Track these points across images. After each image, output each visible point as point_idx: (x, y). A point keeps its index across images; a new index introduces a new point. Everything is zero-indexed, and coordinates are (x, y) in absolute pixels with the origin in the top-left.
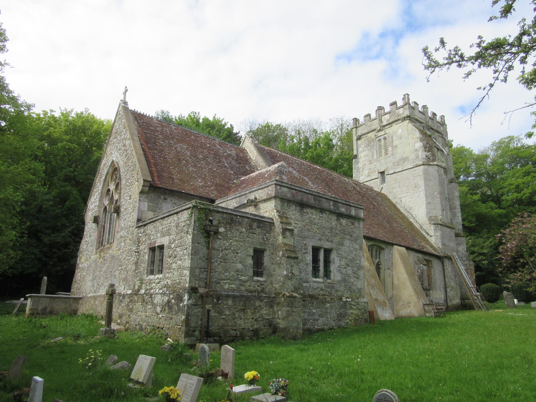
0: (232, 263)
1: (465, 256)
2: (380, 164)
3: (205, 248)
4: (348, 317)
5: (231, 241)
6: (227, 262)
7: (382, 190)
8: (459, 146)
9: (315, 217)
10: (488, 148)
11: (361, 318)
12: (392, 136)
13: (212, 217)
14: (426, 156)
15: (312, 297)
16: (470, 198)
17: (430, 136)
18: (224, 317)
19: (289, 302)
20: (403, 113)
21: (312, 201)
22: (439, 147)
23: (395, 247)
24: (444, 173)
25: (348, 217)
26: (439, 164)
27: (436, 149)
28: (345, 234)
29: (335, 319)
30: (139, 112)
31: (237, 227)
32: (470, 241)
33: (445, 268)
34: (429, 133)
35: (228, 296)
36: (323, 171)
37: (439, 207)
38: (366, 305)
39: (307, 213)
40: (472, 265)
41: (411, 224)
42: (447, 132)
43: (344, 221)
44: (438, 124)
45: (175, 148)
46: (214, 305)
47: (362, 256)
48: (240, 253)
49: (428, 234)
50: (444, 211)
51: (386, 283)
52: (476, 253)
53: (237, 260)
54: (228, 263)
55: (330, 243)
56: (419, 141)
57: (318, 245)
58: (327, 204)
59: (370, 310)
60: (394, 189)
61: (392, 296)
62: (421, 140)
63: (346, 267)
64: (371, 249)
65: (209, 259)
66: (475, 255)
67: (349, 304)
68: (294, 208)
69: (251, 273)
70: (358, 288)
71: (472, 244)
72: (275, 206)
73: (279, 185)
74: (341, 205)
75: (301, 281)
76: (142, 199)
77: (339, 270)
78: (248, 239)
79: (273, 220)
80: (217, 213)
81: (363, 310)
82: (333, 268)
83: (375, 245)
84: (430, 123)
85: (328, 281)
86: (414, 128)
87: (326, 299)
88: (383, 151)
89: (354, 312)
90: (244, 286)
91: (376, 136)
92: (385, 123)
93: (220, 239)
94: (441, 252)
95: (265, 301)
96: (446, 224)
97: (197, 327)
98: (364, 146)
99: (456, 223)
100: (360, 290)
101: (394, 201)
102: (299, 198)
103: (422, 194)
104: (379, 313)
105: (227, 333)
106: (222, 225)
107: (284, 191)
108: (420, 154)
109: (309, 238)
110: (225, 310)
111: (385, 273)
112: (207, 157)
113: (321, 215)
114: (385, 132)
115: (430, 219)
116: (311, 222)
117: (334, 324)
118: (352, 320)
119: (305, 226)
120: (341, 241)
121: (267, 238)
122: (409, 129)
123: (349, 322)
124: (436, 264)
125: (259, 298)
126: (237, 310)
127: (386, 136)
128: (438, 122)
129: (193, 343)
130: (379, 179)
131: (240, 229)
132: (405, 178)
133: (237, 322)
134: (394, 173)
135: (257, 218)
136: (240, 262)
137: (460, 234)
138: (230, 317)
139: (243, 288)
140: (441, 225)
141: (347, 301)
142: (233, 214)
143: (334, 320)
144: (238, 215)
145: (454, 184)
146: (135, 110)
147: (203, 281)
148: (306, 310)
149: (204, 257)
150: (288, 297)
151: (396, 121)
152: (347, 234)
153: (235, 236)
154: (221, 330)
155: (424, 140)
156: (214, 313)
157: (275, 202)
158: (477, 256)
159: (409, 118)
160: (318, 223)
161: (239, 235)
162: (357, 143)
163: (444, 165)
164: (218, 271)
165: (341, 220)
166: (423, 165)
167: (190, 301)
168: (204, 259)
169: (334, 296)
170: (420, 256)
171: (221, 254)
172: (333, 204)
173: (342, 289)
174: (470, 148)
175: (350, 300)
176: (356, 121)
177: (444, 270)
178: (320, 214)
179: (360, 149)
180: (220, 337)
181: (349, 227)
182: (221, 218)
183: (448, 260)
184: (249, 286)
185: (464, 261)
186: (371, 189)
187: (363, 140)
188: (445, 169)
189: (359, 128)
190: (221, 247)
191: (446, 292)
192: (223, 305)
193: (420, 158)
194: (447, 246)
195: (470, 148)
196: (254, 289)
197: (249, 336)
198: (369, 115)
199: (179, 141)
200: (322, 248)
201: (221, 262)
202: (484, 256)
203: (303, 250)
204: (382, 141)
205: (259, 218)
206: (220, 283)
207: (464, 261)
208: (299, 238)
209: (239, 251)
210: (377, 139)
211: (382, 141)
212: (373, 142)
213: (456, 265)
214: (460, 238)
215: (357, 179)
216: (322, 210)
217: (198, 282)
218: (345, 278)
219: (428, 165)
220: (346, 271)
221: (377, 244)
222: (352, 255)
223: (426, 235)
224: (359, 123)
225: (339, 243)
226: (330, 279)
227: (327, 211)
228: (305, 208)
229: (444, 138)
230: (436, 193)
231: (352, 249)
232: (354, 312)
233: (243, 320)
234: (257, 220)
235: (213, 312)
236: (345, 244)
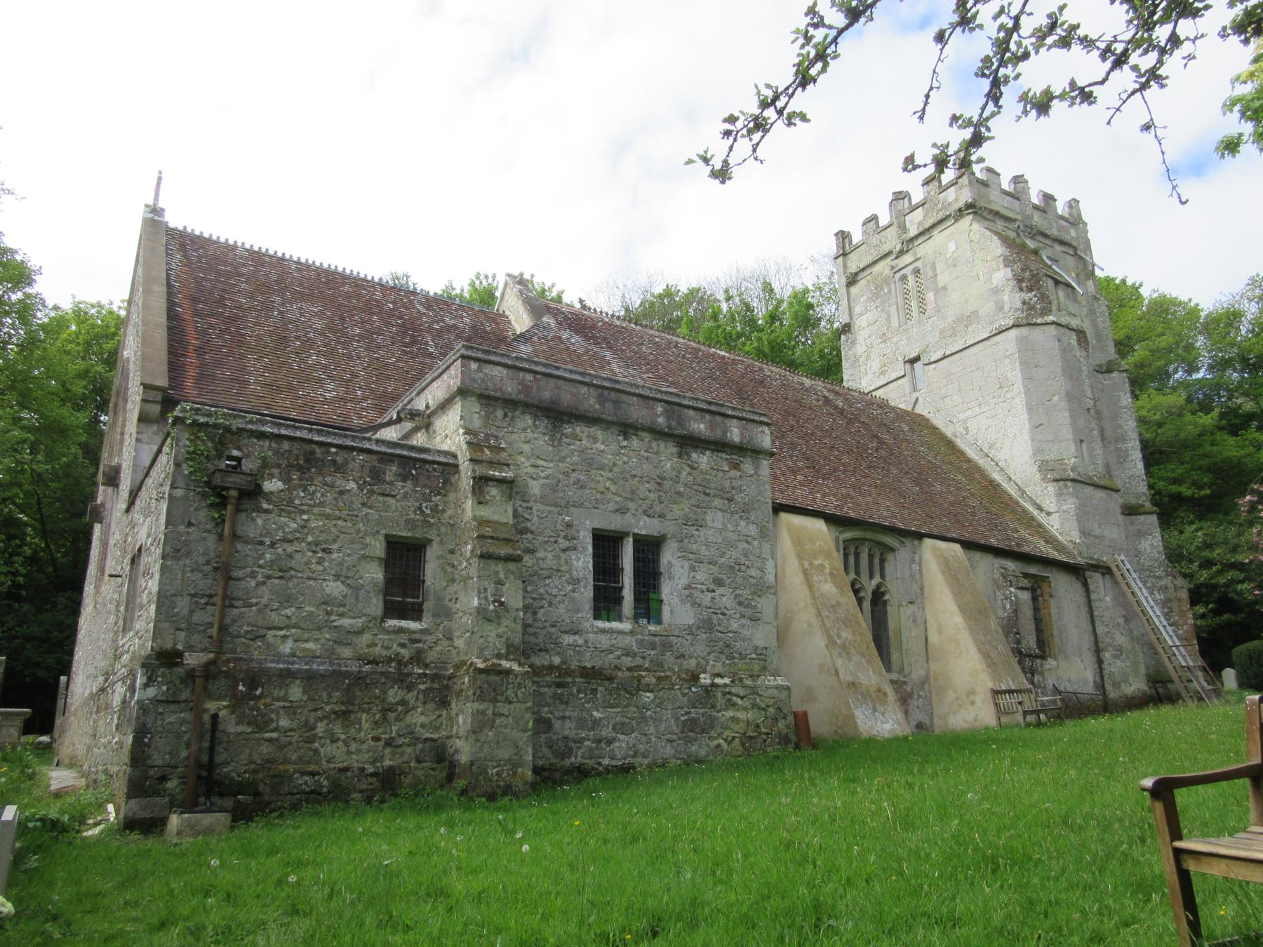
0: (309, 578)
1: (1159, 566)
2: (908, 339)
3: (212, 538)
4: (719, 730)
5: (305, 517)
6: (292, 577)
7: (917, 406)
8: (1156, 295)
9: (602, 447)
10: (1242, 297)
11: (766, 734)
12: (934, 263)
13: (239, 448)
14: (1024, 303)
15: (591, 674)
16: (1190, 423)
17: (1036, 252)
18: (274, 735)
19: (485, 686)
20: (956, 200)
21: (590, 401)
22: (1061, 276)
23: (928, 542)
24: (1079, 344)
25: (720, 446)
26: (1064, 320)
27: (1050, 283)
28: (708, 495)
29: (675, 737)
30: (197, 233)
31: (328, 479)
32: (1199, 534)
33: (1093, 597)
34: (1031, 244)
35: (287, 676)
36: (734, 362)
37: (1067, 433)
38: (783, 695)
39: (575, 437)
40: (1182, 588)
41: (993, 486)
42: (1088, 243)
43: (704, 460)
44: (1062, 222)
45: (281, 313)
46: (237, 703)
47: (769, 557)
48: (339, 550)
49: (1040, 509)
50: (1084, 446)
51: (904, 641)
52: (1216, 564)
53: (325, 569)
54: (295, 581)
55: (655, 521)
56: (1002, 265)
57: (613, 527)
58: (644, 412)
59: (794, 710)
60: (947, 401)
61: (927, 678)
62: (1007, 262)
63: (712, 587)
64: (852, 549)
65: (224, 571)
66: (1214, 569)
67: (724, 694)
68: (530, 422)
69: (376, 606)
70: (756, 648)
71: (1204, 543)
72: (462, 418)
73: (477, 360)
74: (691, 412)
75: (553, 630)
76: (144, 437)
77: (690, 596)
78: (365, 510)
79: (455, 456)
80: (257, 438)
81: (771, 710)
82: (669, 591)
83: (865, 539)
84: (1037, 219)
85: (652, 628)
86: (988, 233)
87: (639, 678)
88: (914, 304)
89: (741, 715)
90: (350, 644)
91: (892, 268)
92: (913, 232)
93: (267, 511)
94: (1080, 553)
95: (422, 687)
96: (1091, 478)
97: (176, 767)
98: (865, 297)
99: (1129, 478)
100: (762, 654)
101: (948, 431)
102: (546, 395)
103: (1019, 403)
104: (859, 722)
105: (282, 783)
106: (276, 471)
107: (492, 377)
108: (1006, 298)
109: (581, 506)
110: (278, 714)
111: (898, 615)
112: (376, 333)
113: (625, 443)
114: (915, 254)
115: (1044, 467)
116: (590, 463)
117: (669, 750)
118: (734, 738)
119: (566, 474)
120: (695, 513)
121: (435, 509)
122: (975, 237)
123: (724, 745)
124: (1064, 590)
125: (403, 680)
126: (319, 713)
127: (919, 264)
128: (1062, 218)
129: (157, 814)
130: (906, 378)
131: (338, 483)
132: (973, 368)
133: (322, 751)
134: (945, 357)
135: (398, 451)
136: (337, 577)
137: (1142, 506)
138: (296, 737)
139: (347, 652)
140: (1073, 480)
141: (713, 685)
142: (311, 442)
143: (671, 741)
144: (331, 445)
145: (1115, 374)
146: (185, 228)
147: (204, 631)
148: (567, 714)
149: (208, 563)
150: (485, 671)
151: (941, 221)
152: (715, 496)
153: (322, 504)
154: (261, 776)
155: (1014, 262)
156: (237, 724)
157: (463, 406)
158: (1220, 572)
159: (971, 208)
160: (615, 464)
161: (335, 499)
162: (848, 293)
163: (1075, 323)
164: (257, 604)
165: (694, 456)
167: (151, 692)
168: (208, 568)
169: (670, 669)
170: (1011, 565)
171: (268, 556)
172: (666, 411)
173: (700, 649)
174: (1190, 300)
175: (727, 680)
176: (843, 239)
177: (1089, 601)
178: (621, 438)
179: (858, 309)
180: (257, 794)
181: (721, 474)
182: (270, 453)
183: (1103, 574)
184: (368, 646)
185: (1160, 578)
186: (883, 405)
187: (862, 283)
188: (1080, 333)
189: (851, 255)
190: (268, 533)
191: (1100, 662)
192: (268, 700)
193: (1006, 308)
194: (1096, 537)
195: (1190, 300)
196: (385, 653)
197: (361, 791)
198: (874, 219)
199: (299, 297)
200: (627, 534)
201: (269, 577)
202: (1241, 570)
203: (561, 540)
204: (909, 278)
205: (405, 453)
206: (264, 636)
207: (1160, 578)
208: (549, 508)
209: (334, 547)
210: (898, 276)
211: (911, 278)
212: (888, 284)
213: (1125, 588)
214: (1142, 518)
215: (854, 385)
216: (627, 429)
217: (183, 634)
218: (710, 619)
219: (1029, 324)
220: (713, 598)
221: (869, 535)
222: (734, 554)
223: (1036, 513)
224: (851, 242)
225: (688, 519)
226: (659, 622)
227: (643, 429)
228: (568, 422)
229: (1081, 258)
230: (1055, 398)
231: (733, 536)
232: (741, 715)
233: (340, 743)
234: (399, 456)
235: (233, 722)
236: (710, 524)
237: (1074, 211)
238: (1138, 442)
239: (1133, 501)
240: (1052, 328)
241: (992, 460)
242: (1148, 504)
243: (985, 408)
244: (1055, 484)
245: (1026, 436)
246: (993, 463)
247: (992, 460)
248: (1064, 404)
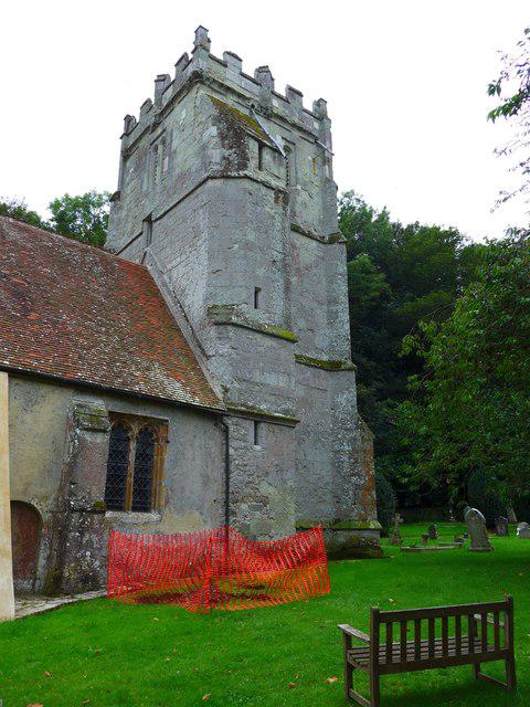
14: (224, 158)
211: (160, 148)
219: (223, 177)
230: (236, 246)
242: (350, 363)
243: (184, 257)
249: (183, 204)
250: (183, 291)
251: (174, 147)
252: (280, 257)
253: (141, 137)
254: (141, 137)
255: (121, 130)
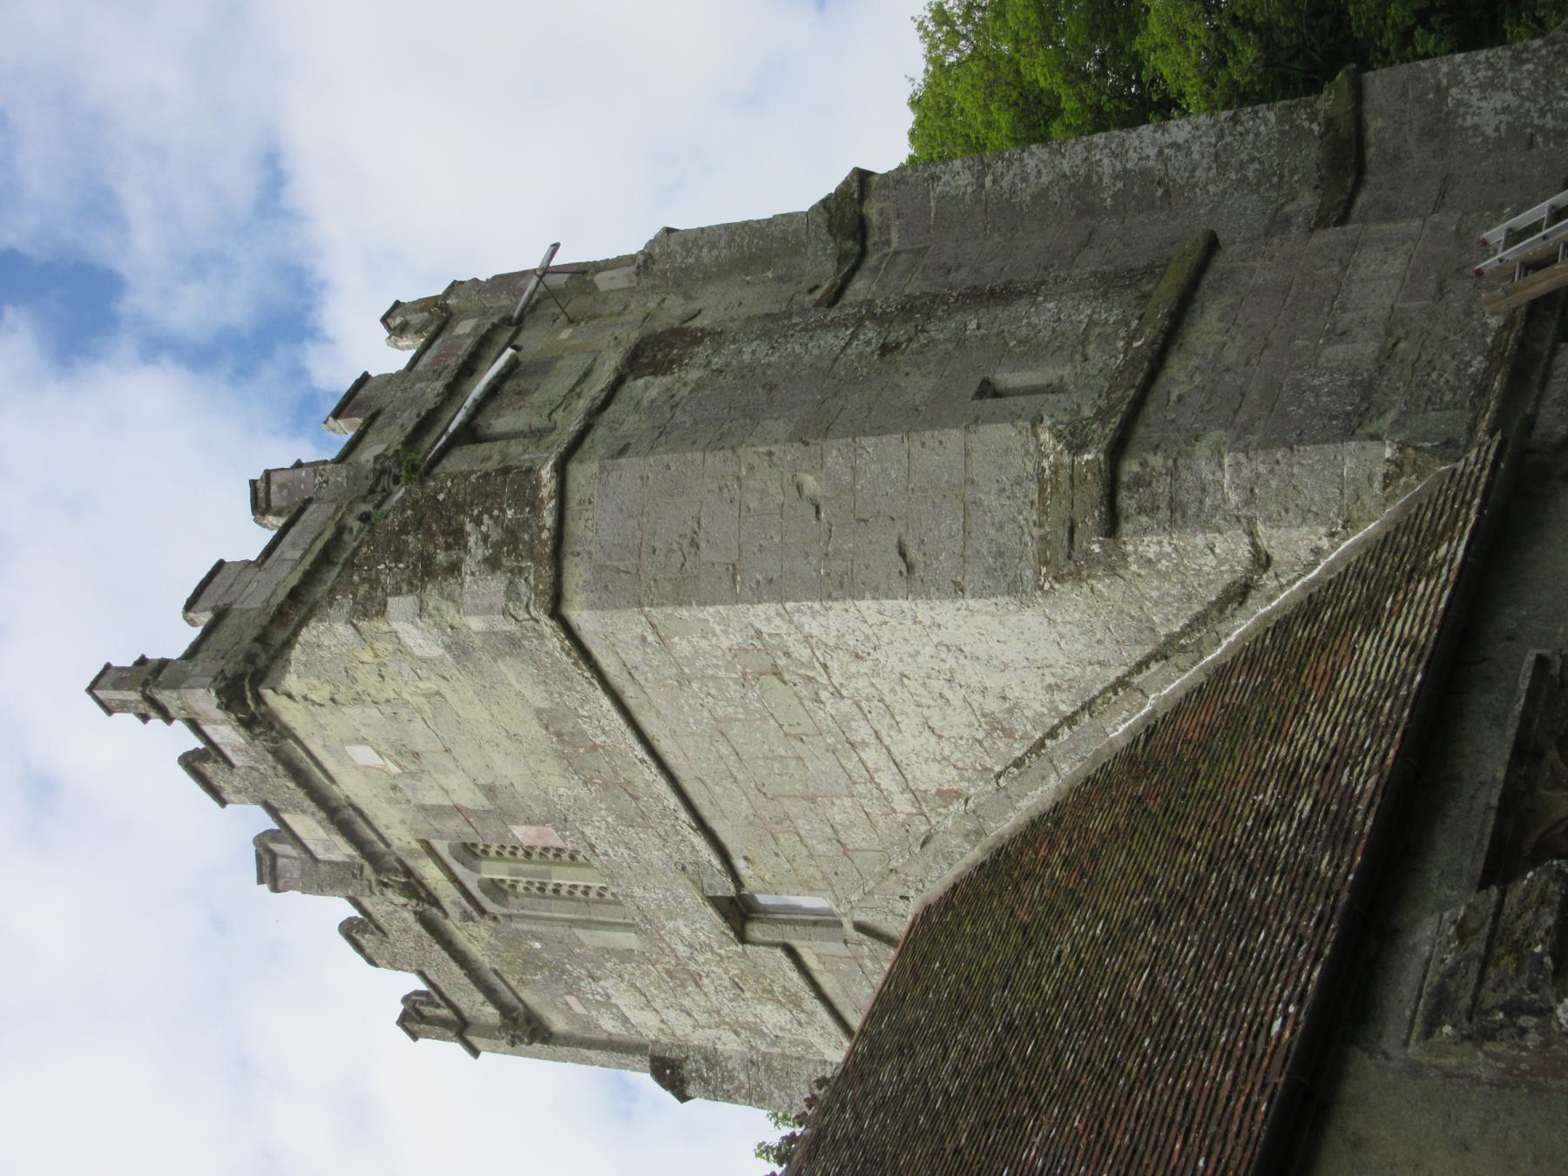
2: (671, 916)
12: (424, 809)
14: (493, 564)
44: (426, 359)
49: (1240, 593)
50: (1007, 378)
60: (856, 838)
62: (371, 608)
96: (1131, 363)
99: (1222, 167)
127: (442, 847)
137: (1330, 123)
140: (1117, 449)
155: (374, 583)
166: (556, 612)
187: (530, 997)
193: (510, 627)
194: (1387, 355)
211: (493, 871)
214: (1375, 124)
229: (531, 308)
230: (810, 482)
237: (416, 319)
238: (1099, 139)
239: (1311, 154)
240: (582, 473)
241: (1053, 733)
242: (1325, 102)
243: (862, 731)
244: (1126, 527)
245: (946, 611)
246: (1065, 733)
247: (1053, 733)
248: (835, 454)
249: (665, 746)
250: (995, 726)
251: (472, 799)
252: (870, 332)
253: (461, 958)
254: (461, 958)
255: (445, 1052)
